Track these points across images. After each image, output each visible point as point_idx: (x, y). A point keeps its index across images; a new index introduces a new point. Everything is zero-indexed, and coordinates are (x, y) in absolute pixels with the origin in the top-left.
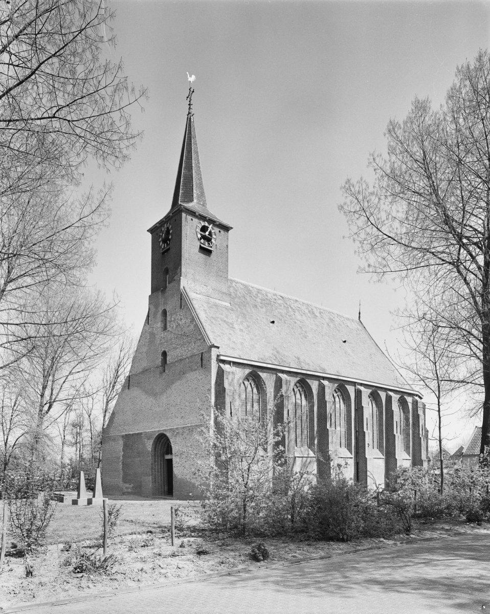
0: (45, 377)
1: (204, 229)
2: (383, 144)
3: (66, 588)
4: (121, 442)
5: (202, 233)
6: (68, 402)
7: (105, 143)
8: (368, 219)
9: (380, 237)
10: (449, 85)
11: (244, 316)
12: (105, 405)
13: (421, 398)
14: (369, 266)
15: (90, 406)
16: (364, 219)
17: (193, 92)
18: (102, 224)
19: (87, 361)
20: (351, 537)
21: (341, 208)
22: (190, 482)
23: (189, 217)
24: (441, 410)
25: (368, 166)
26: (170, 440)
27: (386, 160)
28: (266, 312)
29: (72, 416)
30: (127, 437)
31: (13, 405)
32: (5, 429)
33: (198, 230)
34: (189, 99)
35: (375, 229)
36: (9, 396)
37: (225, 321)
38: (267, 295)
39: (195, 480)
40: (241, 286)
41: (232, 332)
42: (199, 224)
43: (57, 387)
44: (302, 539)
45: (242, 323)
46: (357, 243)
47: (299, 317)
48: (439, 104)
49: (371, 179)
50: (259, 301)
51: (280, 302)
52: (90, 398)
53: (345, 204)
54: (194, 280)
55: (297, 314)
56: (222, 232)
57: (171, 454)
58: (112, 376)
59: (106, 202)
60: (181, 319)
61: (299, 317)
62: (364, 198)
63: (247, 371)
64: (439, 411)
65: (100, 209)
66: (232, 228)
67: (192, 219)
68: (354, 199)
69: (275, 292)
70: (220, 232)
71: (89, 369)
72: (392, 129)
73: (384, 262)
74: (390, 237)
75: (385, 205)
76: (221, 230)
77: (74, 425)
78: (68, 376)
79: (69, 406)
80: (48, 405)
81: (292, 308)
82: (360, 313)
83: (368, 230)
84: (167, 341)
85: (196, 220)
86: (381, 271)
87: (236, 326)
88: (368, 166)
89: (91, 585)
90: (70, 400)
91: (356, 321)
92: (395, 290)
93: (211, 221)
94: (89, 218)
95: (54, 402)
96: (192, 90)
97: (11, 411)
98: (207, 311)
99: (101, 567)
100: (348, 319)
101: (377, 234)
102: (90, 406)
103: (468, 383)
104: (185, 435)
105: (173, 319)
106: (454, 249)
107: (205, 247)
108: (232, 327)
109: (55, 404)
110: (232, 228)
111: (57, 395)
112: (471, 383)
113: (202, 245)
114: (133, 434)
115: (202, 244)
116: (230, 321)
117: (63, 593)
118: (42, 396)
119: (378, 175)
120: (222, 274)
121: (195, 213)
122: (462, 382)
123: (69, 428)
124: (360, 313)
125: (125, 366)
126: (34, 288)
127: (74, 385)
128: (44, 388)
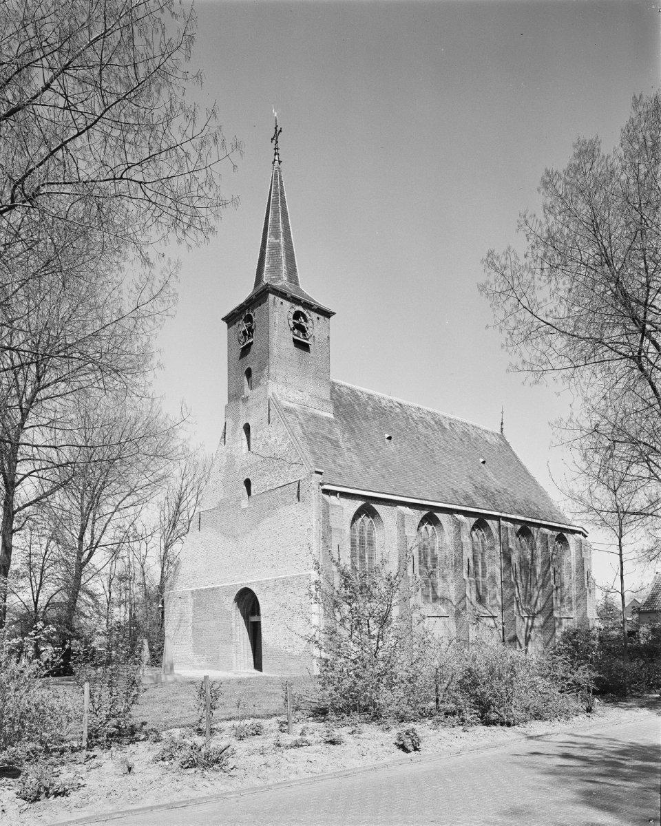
0: (85, 517)
1: (297, 315)
2: (537, 201)
3: (179, 787)
4: (190, 600)
5: (296, 321)
6: (115, 547)
7: (182, 213)
8: (519, 300)
9: (536, 324)
10: (624, 122)
11: (352, 431)
12: (163, 551)
13: (585, 536)
14: (524, 362)
15: (143, 552)
16: (513, 301)
17: (280, 131)
18: (165, 313)
19: (138, 492)
20: (519, 720)
21: (482, 288)
22: (286, 652)
23: (279, 300)
24: (623, 553)
25: (517, 231)
26: (258, 596)
27: (544, 223)
28: (380, 425)
29: (119, 567)
30: (197, 594)
31: (44, 551)
32: (34, 584)
33: (291, 316)
34: (274, 141)
35: (529, 314)
36: (37, 540)
37: (327, 438)
38: (380, 402)
39: (292, 649)
40: (346, 391)
41: (336, 452)
42: (288, 309)
43: (99, 526)
44: (455, 724)
45: (349, 439)
46: (505, 332)
47: (422, 430)
48: (612, 146)
49: (521, 245)
50: (370, 409)
51: (398, 410)
52: (143, 542)
53: (487, 282)
54: (286, 384)
55: (420, 426)
56: (322, 317)
57: (259, 614)
58: (172, 512)
59: (171, 284)
60: (270, 437)
61: (422, 430)
62: (513, 272)
63: (360, 503)
64: (621, 555)
65: (163, 294)
66: (334, 314)
67: (282, 303)
68: (499, 276)
69: (390, 398)
70: (318, 318)
71: (144, 501)
72: (548, 182)
73: (544, 358)
74: (548, 324)
75: (540, 281)
76: (320, 316)
77: (122, 578)
78: (113, 513)
79: (115, 552)
80: (88, 552)
81: (413, 419)
82: (502, 424)
83: (520, 316)
84: (250, 466)
85: (287, 304)
86: (539, 370)
87: (341, 443)
88: (517, 231)
89: (208, 784)
90: (117, 546)
91: (498, 434)
92: (558, 394)
93: (308, 306)
94: (149, 305)
95: (96, 547)
96: (278, 129)
97: (41, 562)
98: (304, 425)
99: (217, 761)
100: (487, 432)
101: (531, 320)
102: (143, 552)
103: (648, 515)
104: (277, 590)
105: (258, 437)
106: (635, 340)
107: (299, 339)
108: (338, 446)
109: (97, 550)
110: (334, 314)
111: (100, 539)
112: (651, 514)
113: (296, 338)
114: (206, 590)
115: (296, 335)
116: (334, 438)
117: (176, 793)
118: (81, 539)
119: (531, 241)
120: (322, 373)
121: (286, 294)
122: (639, 513)
123: (115, 581)
124: (502, 424)
125: (188, 499)
126: (70, 397)
127: (121, 525)
128: (83, 528)
